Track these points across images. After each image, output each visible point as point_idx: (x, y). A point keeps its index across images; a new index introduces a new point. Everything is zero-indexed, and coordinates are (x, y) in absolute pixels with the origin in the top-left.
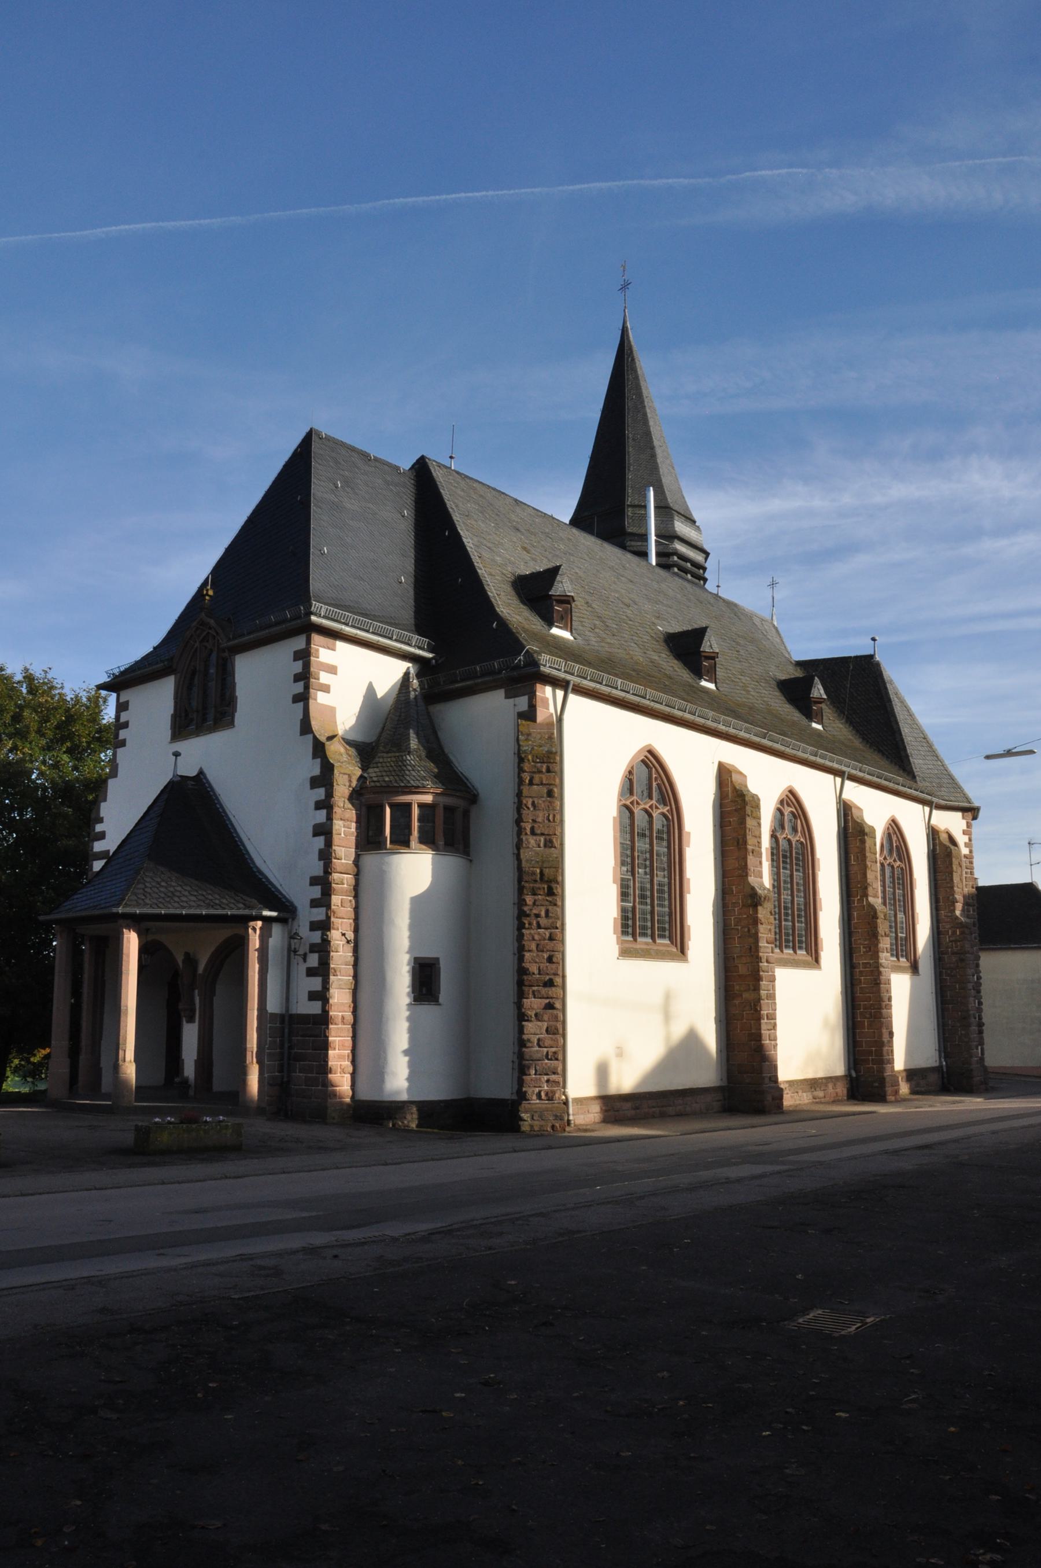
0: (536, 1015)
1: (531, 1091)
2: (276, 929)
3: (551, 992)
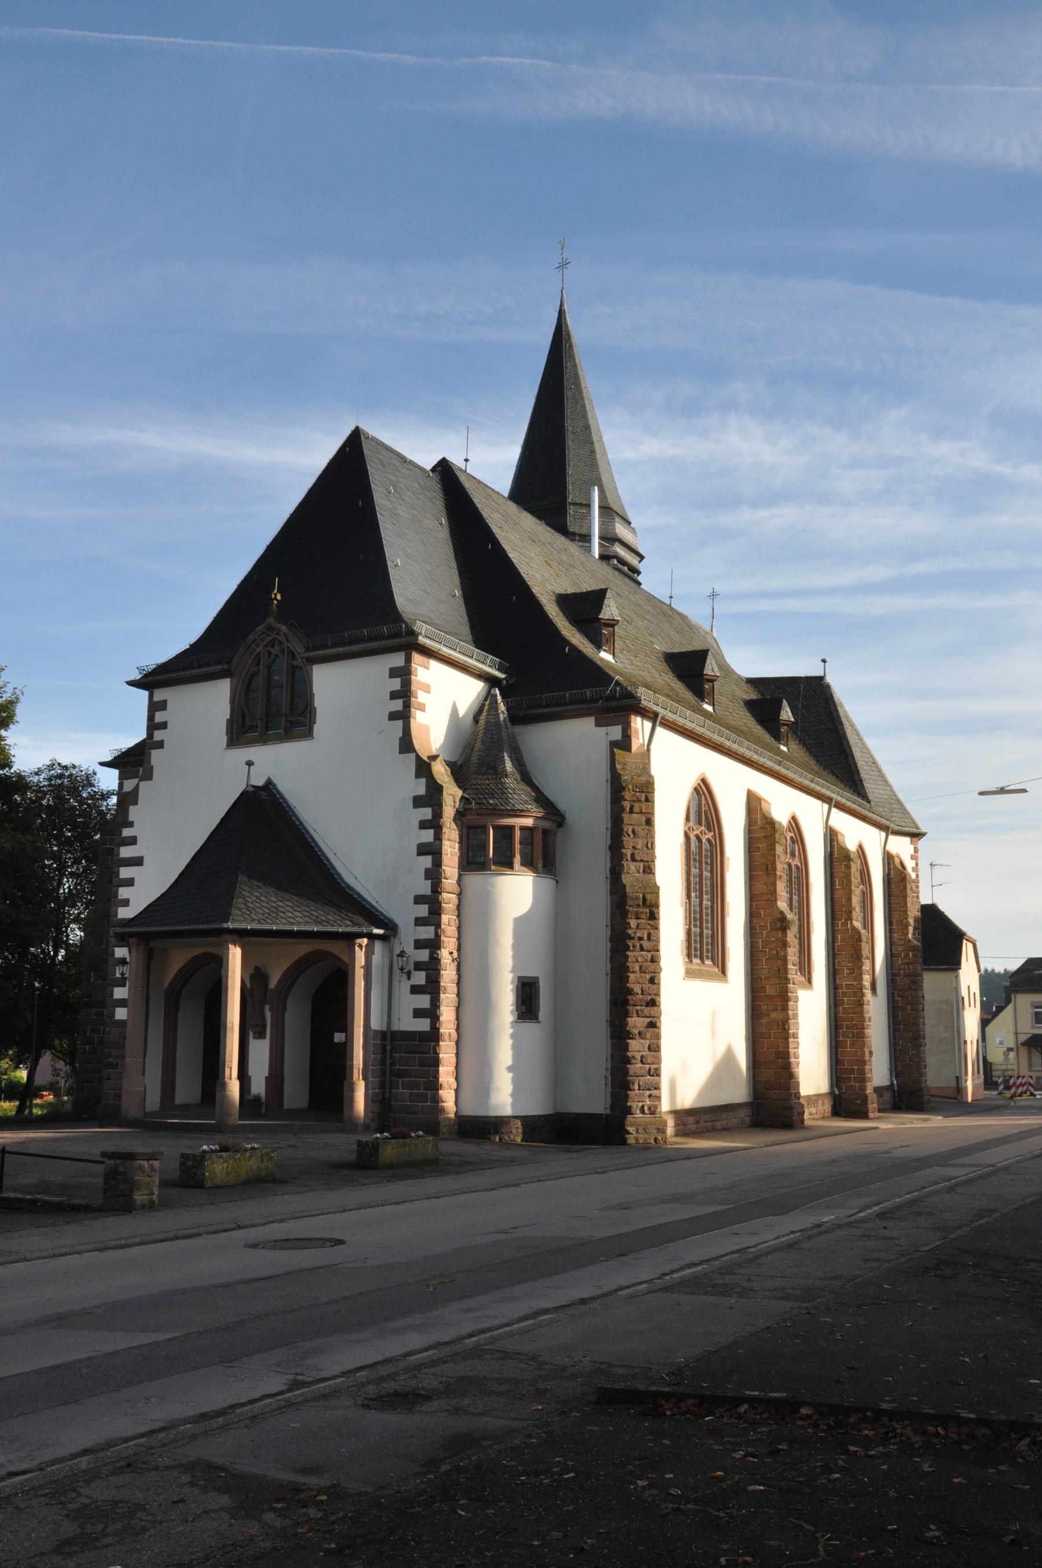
0: (640, 1033)
1: (635, 1105)
2: (378, 945)
3: (653, 1010)
